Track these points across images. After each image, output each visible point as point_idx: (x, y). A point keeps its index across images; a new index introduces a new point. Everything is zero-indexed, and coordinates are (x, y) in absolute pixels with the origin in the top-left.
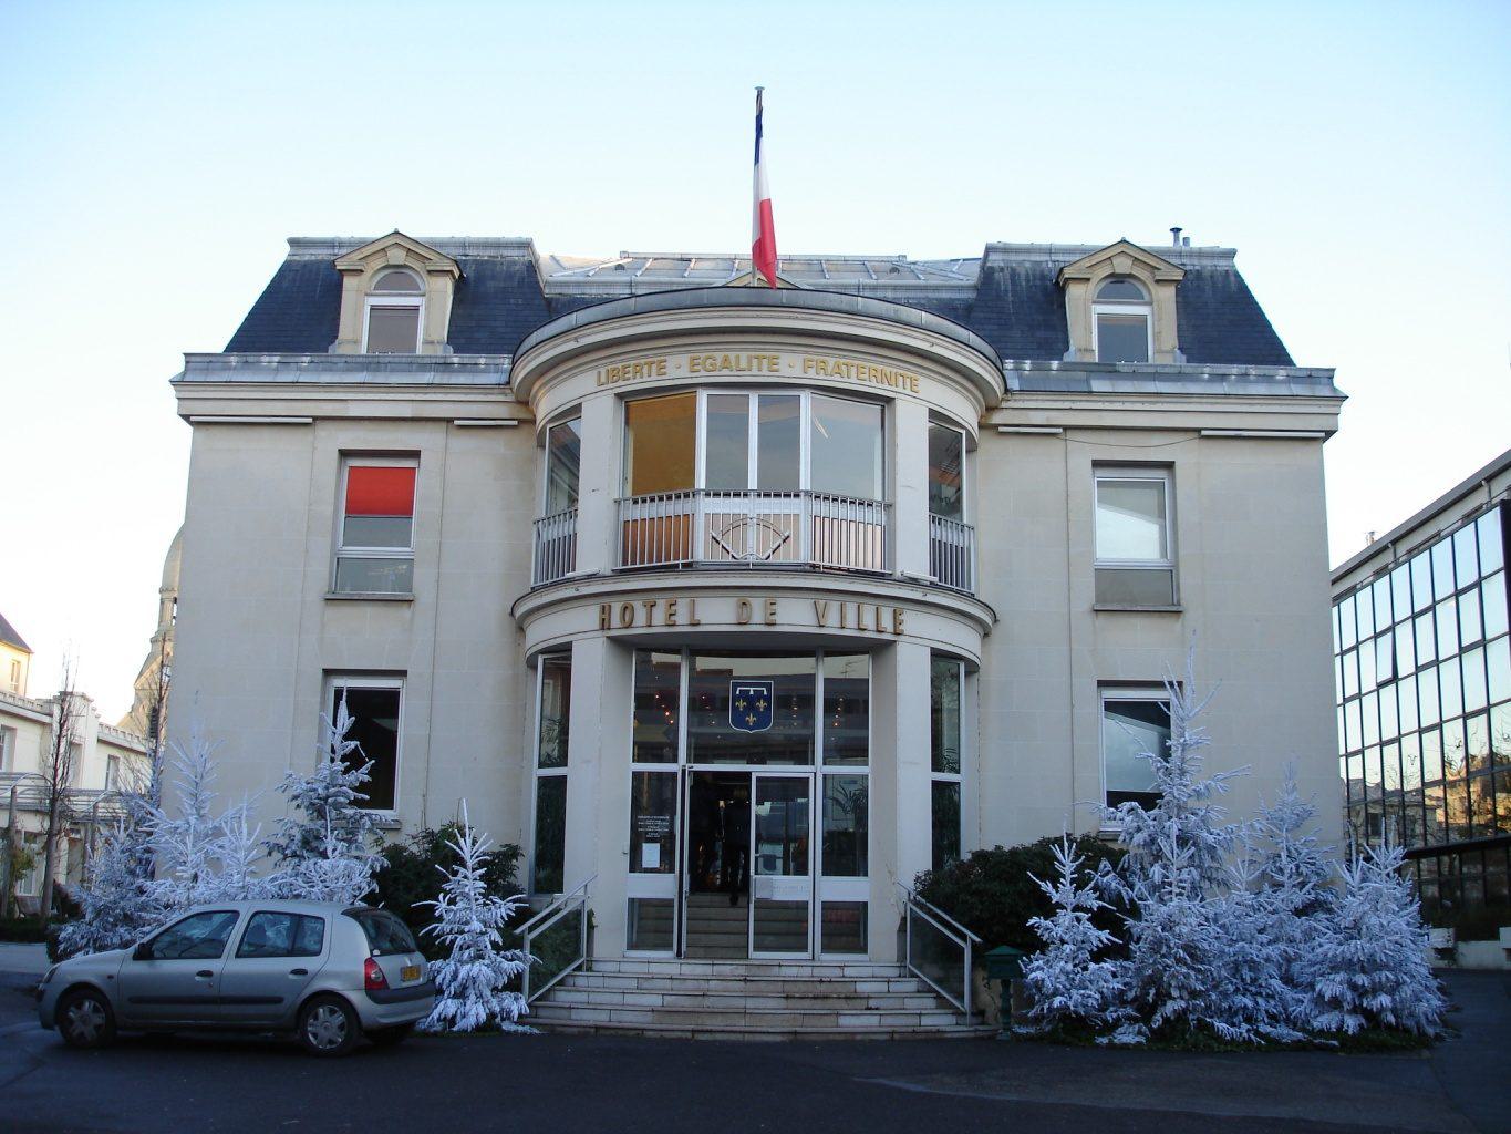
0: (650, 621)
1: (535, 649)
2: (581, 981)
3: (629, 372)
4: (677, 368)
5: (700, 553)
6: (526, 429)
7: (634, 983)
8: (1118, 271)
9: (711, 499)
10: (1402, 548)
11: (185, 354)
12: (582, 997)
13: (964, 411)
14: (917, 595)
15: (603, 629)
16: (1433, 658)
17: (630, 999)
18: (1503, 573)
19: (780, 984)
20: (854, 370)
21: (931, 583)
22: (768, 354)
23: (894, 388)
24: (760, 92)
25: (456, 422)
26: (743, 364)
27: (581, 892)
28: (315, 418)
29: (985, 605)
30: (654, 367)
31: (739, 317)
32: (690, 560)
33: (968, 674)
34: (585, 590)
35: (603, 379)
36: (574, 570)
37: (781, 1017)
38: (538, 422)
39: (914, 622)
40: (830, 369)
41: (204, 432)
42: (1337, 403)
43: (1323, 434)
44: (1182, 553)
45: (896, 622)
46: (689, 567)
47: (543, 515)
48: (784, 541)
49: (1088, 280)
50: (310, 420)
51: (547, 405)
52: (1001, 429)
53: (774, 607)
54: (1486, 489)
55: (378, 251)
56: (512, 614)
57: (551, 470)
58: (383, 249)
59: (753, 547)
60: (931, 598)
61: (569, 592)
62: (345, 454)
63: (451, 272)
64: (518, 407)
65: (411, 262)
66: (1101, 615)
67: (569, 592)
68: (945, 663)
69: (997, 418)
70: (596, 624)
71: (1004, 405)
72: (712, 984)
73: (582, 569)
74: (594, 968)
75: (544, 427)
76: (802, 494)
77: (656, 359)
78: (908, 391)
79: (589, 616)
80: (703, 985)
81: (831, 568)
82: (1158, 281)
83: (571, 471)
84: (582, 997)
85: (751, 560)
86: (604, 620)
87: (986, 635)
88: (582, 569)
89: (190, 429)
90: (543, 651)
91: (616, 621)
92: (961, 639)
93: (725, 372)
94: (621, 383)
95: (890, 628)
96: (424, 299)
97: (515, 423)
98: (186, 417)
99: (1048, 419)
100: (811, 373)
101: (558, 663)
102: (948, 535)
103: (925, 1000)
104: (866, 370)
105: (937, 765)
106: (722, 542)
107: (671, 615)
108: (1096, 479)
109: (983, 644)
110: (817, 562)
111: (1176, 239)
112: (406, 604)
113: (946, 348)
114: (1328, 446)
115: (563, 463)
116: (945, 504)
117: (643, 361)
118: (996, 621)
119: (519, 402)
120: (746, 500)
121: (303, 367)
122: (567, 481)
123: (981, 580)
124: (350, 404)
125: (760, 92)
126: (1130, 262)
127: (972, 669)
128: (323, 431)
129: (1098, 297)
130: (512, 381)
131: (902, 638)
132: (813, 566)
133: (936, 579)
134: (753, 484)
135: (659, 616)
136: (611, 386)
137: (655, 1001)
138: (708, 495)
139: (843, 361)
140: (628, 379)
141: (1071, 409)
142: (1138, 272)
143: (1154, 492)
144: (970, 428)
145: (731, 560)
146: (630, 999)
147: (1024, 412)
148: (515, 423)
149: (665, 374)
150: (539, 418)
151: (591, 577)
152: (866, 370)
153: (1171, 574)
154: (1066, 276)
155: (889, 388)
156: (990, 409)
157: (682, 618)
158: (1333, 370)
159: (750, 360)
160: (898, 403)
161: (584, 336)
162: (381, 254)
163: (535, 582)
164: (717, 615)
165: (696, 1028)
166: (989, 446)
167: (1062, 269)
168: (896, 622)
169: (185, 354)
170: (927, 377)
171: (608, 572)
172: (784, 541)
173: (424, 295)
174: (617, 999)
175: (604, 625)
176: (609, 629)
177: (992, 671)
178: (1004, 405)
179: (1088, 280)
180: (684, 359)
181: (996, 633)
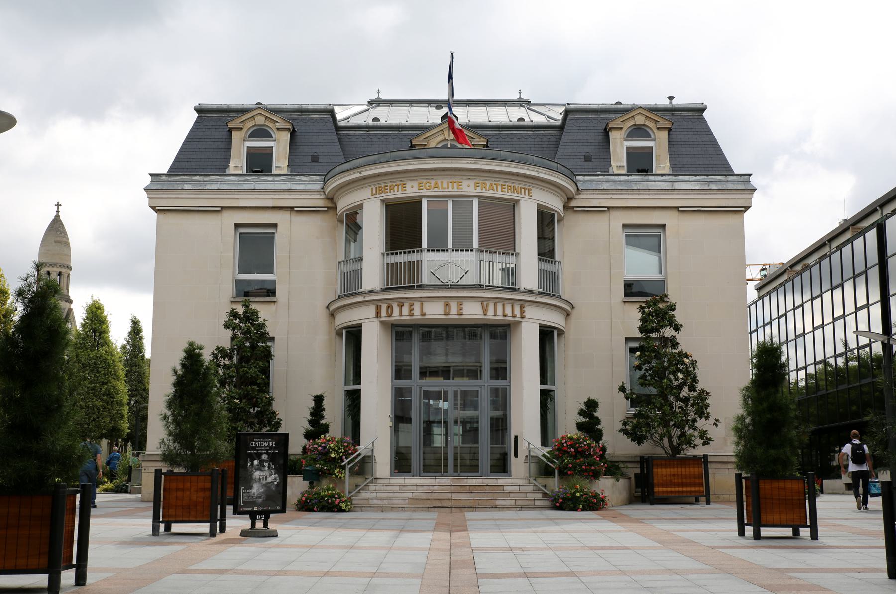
0: (401, 315)
1: (341, 326)
2: (372, 487)
3: (387, 189)
4: (411, 189)
5: (426, 279)
6: (331, 212)
7: (398, 488)
8: (637, 123)
9: (430, 253)
10: (835, 244)
11: (151, 175)
12: (374, 495)
13: (555, 204)
14: (532, 299)
15: (378, 317)
16: (865, 303)
17: (397, 495)
18: (877, 266)
19: (468, 487)
20: (499, 187)
21: (539, 292)
22: (457, 180)
23: (520, 195)
24: (452, 55)
25: (295, 209)
26: (445, 185)
27: (371, 445)
28: (222, 208)
29: (567, 301)
30: (400, 187)
31: (442, 163)
32: (420, 284)
33: (558, 335)
34: (368, 298)
35: (374, 192)
36: (361, 288)
37: (469, 501)
38: (338, 210)
39: (530, 312)
40: (488, 187)
41: (162, 216)
42: (752, 192)
43: (743, 209)
44: (668, 271)
45: (522, 312)
46: (420, 287)
47: (344, 259)
48: (466, 273)
49: (621, 129)
50: (219, 209)
51: (345, 203)
52: (576, 209)
53: (461, 306)
54: (880, 212)
55: (251, 117)
56: (327, 308)
57: (347, 233)
58: (253, 117)
59: (451, 276)
60: (539, 300)
61: (360, 299)
62: (237, 226)
63: (289, 129)
64: (327, 201)
65: (268, 123)
66: (627, 304)
67: (360, 299)
68: (547, 335)
69: (573, 204)
70: (374, 315)
71: (577, 196)
72: (436, 487)
73: (366, 286)
74: (377, 482)
75: (343, 213)
76: (474, 250)
77: (401, 183)
78: (527, 196)
79: (371, 311)
80: (431, 487)
81: (489, 286)
82: (658, 129)
83: (355, 232)
84: (374, 495)
85: (450, 283)
86: (378, 313)
87: (568, 315)
88: (366, 286)
89: (156, 214)
90: (345, 328)
91: (384, 313)
92: (554, 319)
93: (436, 189)
94: (383, 194)
95: (519, 315)
96: (275, 142)
97: (326, 209)
98: (153, 208)
99: (600, 203)
100: (479, 189)
101: (354, 335)
102: (547, 266)
103: (537, 494)
104: (506, 187)
105: (543, 381)
106: (440, 279)
107: (411, 310)
108: (625, 233)
109: (566, 319)
110: (482, 283)
111: (671, 103)
112: (273, 304)
113: (546, 174)
114: (746, 215)
115: (351, 228)
116: (546, 252)
117: (394, 184)
118: (573, 308)
119: (328, 199)
120: (447, 253)
121: (214, 182)
122: (353, 237)
123: (566, 288)
124: (241, 200)
125: (452, 55)
126: (643, 118)
127: (561, 333)
128: (226, 214)
129: (627, 137)
130: (325, 188)
131: (525, 320)
132: (481, 285)
133: (541, 290)
134: (450, 245)
135: (405, 311)
136: (378, 195)
137: (410, 495)
138: (428, 250)
139: (494, 182)
140: (387, 192)
141: (611, 198)
142: (647, 123)
143: (656, 239)
144: (559, 211)
145: (440, 283)
146: (397, 495)
147: (590, 200)
148: (326, 209)
149: (405, 190)
150: (339, 209)
151: (370, 292)
152: (506, 187)
153: (662, 283)
154: (610, 127)
155: (518, 195)
156: (570, 199)
157: (417, 311)
158: (750, 175)
159: (448, 183)
160: (521, 202)
161: (365, 171)
162: (252, 119)
163: (341, 293)
164: (434, 312)
165: (429, 506)
166: (572, 220)
167: (608, 124)
168: (522, 312)
169: (151, 175)
170: (536, 187)
171: (378, 289)
172: (466, 273)
173: (275, 141)
174: (391, 495)
175: (378, 315)
176: (381, 317)
177: (571, 335)
178: (577, 196)
179: (621, 129)
180: (415, 184)
181: (574, 314)
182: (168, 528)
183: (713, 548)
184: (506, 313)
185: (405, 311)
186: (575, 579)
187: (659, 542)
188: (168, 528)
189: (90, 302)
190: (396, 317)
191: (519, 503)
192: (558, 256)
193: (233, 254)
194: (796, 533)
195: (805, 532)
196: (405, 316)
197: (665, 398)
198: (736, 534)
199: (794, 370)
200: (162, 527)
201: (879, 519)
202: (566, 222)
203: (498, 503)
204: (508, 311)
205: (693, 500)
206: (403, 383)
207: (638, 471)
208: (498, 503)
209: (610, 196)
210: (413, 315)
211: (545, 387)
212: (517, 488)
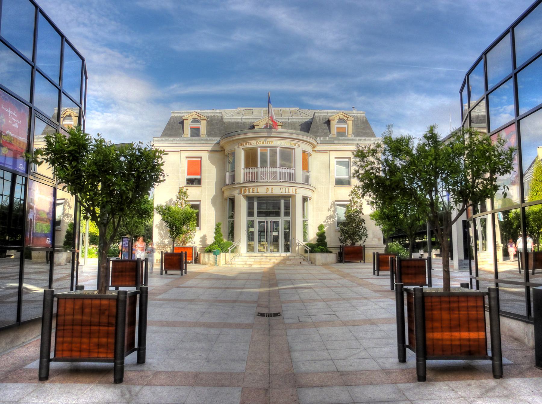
17: (248, 260)
35: (239, 145)
45: (296, 191)
63: (206, 120)
68: (305, 199)
101: (232, 201)
130: (220, 143)
168: (296, 191)
182: (166, 272)
183: (362, 279)
184: (293, 192)
185: (251, 190)
186: (311, 289)
187: (343, 277)
188: (166, 272)
189: (67, 230)
190: (247, 194)
191: (294, 263)
192: (310, 170)
193: (518, 87)
194: (361, 262)
195: (362, 261)
196: (251, 193)
197: (129, 176)
198: (373, 274)
199: (5, 161)
200: (164, 272)
201: (522, 301)
202: (313, 156)
203: (286, 263)
204: (290, 191)
205: (359, 261)
206: (251, 218)
207: (339, 251)
208: (286, 263)
209: (330, 146)
210: (254, 192)
211: (304, 219)
212: (294, 258)
